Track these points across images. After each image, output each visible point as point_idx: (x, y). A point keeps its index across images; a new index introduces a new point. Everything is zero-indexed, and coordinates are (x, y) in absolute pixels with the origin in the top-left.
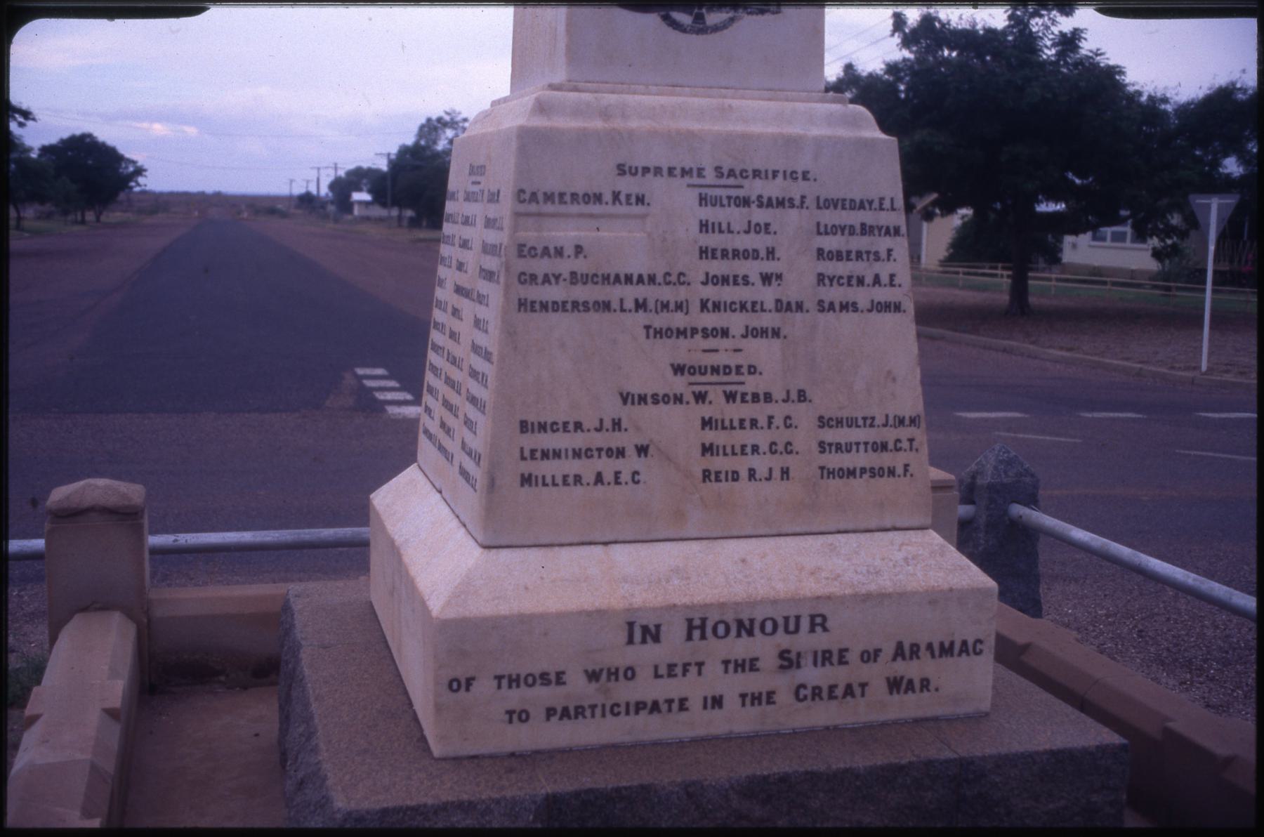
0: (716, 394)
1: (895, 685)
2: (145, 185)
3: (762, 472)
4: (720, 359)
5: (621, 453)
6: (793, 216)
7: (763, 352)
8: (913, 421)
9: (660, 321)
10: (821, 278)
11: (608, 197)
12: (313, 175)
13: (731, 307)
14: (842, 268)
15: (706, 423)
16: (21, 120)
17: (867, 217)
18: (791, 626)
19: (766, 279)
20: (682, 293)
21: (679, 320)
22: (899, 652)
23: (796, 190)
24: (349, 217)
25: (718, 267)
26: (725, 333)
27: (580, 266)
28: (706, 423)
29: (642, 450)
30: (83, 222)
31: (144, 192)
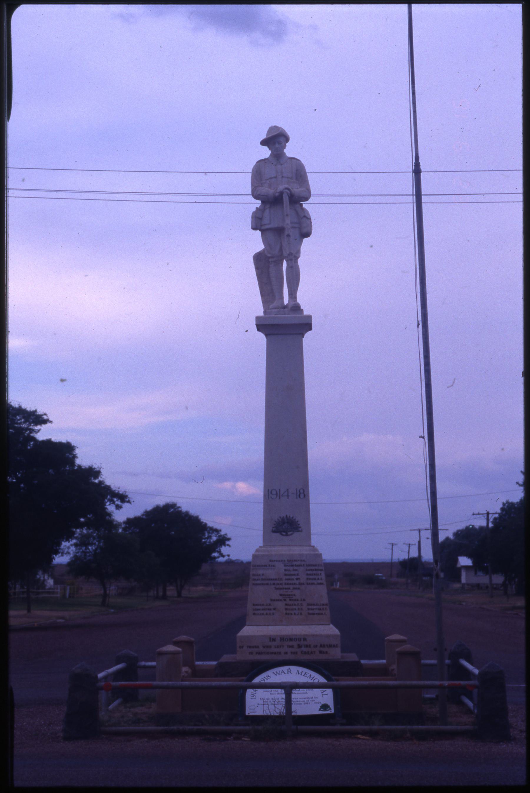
0: (288, 599)
1: (321, 652)
2: (228, 556)
3: (297, 613)
4: (289, 593)
5: (270, 609)
6: (302, 568)
7: (297, 592)
8: (326, 605)
9: (278, 586)
10: (307, 579)
11: (268, 565)
12: (414, 538)
13: (290, 584)
14: (311, 577)
15: (286, 605)
16: (118, 503)
17: (316, 568)
18: (300, 640)
19: (297, 579)
20: (281, 582)
21: (281, 587)
22: (321, 646)
23: (302, 563)
24: (457, 586)
25: (288, 577)
26: (289, 589)
27: (263, 577)
28: (286, 605)
29: (274, 609)
30: (165, 597)
31: (230, 562)
